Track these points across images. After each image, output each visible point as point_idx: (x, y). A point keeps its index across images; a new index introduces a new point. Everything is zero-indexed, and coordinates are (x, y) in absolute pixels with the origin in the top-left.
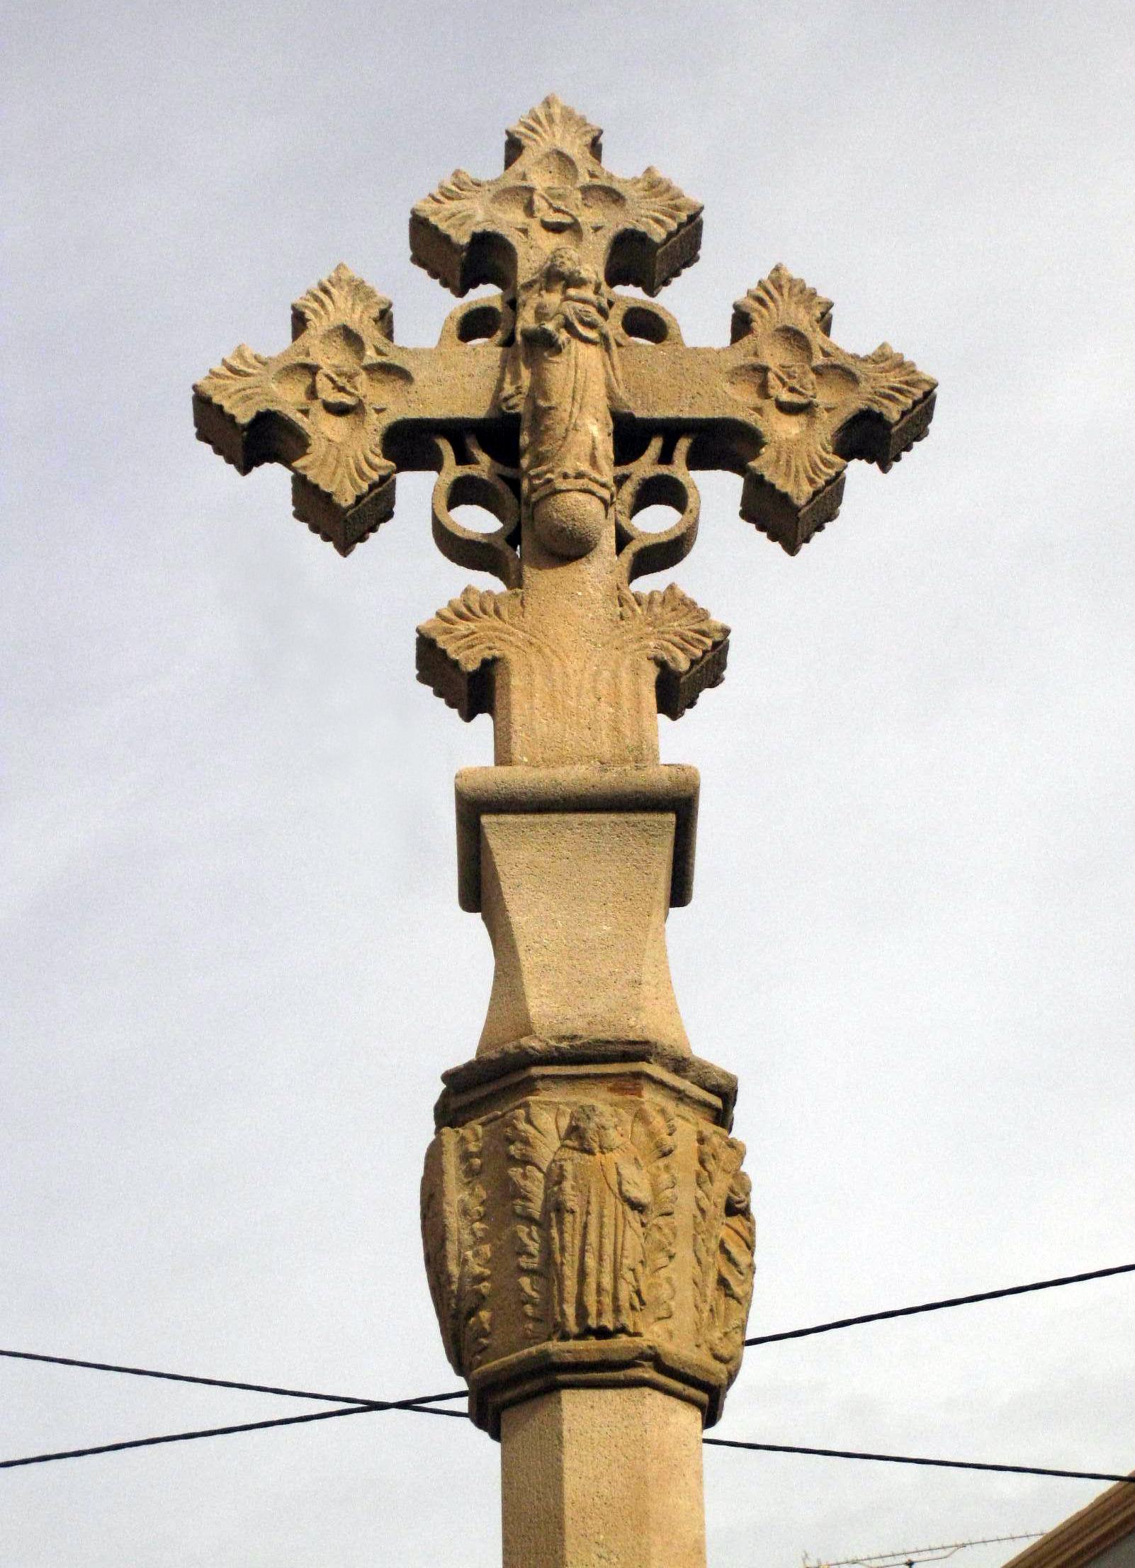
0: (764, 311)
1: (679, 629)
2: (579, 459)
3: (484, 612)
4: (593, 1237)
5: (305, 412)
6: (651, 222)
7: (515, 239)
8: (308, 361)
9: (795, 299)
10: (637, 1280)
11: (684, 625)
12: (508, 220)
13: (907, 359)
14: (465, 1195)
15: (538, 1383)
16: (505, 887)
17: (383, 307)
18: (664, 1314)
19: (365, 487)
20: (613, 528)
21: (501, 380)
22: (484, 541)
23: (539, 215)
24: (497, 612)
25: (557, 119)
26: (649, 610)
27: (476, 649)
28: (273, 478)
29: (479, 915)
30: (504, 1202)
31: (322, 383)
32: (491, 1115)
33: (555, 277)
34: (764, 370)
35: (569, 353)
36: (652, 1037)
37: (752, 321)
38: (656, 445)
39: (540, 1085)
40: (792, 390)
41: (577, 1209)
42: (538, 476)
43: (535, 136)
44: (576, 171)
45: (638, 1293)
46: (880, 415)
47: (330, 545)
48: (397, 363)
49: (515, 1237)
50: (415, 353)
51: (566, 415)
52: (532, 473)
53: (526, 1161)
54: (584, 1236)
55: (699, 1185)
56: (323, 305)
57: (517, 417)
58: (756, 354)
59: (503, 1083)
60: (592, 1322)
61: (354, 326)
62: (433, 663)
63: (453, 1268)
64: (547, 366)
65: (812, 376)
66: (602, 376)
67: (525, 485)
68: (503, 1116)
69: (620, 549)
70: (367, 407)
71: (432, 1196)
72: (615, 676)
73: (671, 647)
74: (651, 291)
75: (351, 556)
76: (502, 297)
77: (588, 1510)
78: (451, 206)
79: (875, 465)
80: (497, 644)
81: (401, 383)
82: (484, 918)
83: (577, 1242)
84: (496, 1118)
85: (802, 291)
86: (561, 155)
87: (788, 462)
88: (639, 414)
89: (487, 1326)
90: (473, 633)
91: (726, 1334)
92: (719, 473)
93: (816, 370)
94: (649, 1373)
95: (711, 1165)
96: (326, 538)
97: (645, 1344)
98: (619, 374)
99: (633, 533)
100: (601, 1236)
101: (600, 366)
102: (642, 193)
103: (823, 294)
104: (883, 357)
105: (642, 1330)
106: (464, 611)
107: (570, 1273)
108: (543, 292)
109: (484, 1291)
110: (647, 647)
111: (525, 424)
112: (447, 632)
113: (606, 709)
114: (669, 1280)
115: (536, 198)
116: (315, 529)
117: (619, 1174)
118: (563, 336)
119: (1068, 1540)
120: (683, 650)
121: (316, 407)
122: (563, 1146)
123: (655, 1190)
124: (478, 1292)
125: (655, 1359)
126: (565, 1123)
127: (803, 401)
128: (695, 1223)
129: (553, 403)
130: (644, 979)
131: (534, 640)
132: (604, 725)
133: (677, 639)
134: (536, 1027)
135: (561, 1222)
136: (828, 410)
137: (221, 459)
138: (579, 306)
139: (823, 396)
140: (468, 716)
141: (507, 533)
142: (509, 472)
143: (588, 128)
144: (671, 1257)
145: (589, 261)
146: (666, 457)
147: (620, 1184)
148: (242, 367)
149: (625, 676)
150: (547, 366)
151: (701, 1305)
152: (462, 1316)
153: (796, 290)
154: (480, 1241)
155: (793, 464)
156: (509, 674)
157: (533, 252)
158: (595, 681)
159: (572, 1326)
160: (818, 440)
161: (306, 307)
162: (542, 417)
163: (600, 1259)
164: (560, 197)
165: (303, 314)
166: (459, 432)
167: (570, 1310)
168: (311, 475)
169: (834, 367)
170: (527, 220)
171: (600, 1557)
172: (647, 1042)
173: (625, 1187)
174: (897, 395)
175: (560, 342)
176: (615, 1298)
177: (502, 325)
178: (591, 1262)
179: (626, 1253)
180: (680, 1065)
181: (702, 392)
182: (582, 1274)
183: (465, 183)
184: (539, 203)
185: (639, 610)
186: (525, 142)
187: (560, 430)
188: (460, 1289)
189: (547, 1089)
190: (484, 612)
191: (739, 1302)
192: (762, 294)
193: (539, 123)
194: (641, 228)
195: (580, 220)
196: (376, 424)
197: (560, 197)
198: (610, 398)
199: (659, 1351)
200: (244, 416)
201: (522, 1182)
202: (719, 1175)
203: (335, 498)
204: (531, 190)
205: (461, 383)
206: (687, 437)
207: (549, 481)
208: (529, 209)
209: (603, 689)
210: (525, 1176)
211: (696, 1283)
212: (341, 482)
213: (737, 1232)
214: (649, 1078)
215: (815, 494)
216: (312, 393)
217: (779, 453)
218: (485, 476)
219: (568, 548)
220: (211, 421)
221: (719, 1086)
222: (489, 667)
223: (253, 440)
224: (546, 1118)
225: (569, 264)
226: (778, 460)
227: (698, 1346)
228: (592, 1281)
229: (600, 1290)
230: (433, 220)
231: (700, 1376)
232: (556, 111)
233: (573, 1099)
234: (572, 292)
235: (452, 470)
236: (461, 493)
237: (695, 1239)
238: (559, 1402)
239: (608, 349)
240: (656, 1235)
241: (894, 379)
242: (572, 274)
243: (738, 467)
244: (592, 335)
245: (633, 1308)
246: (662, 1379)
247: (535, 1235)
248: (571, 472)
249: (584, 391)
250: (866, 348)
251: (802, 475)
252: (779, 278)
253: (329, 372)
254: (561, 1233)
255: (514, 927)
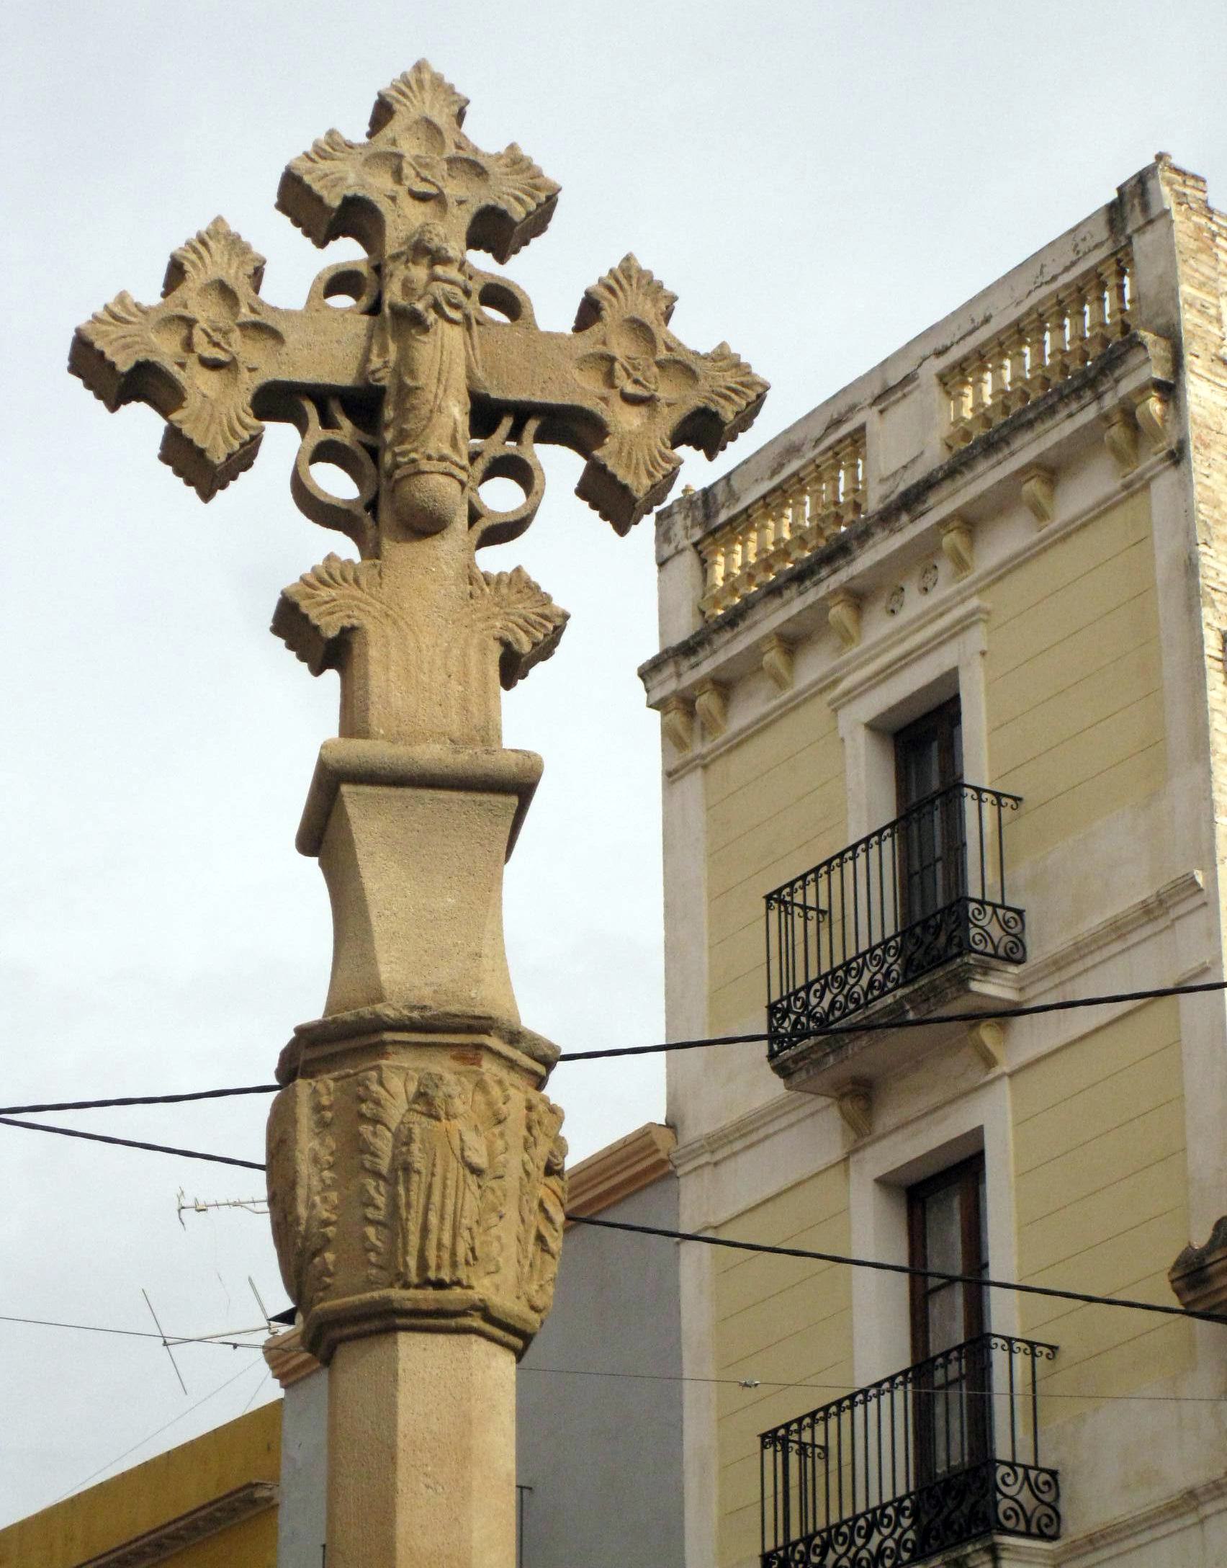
0: (613, 299)
1: (524, 612)
2: (440, 440)
3: (345, 580)
4: (436, 1198)
5: (182, 365)
6: (512, 200)
7: (384, 206)
8: (186, 313)
9: (642, 290)
10: (472, 1238)
11: (527, 608)
12: (377, 186)
13: (743, 360)
14: (315, 1144)
15: (376, 1324)
16: (361, 854)
17: (257, 264)
18: (492, 1269)
19: (236, 445)
20: (466, 507)
21: (368, 351)
22: (344, 507)
23: (407, 183)
24: (356, 581)
25: (427, 84)
26: (497, 590)
27: (335, 616)
28: (142, 422)
29: (315, 860)
30: (353, 1154)
31: (198, 336)
32: (343, 1073)
33: (423, 251)
34: (612, 360)
35: (436, 334)
36: (495, 1013)
37: (601, 309)
38: (507, 424)
39: (390, 1049)
40: (636, 382)
41: (424, 1171)
42: (403, 454)
43: (405, 100)
44: (443, 142)
45: (473, 1250)
46: (716, 415)
47: (192, 490)
48: (270, 323)
49: (363, 1190)
50: (288, 314)
51: (431, 397)
52: (397, 449)
53: (376, 1121)
54: (429, 1196)
55: (526, 1149)
56: (201, 258)
57: (382, 391)
58: (604, 343)
59: (353, 1043)
60: (432, 1275)
61: (230, 282)
62: (291, 622)
63: (302, 1211)
64: (415, 344)
65: (655, 369)
66: (463, 354)
67: (387, 458)
68: (356, 1074)
69: (471, 524)
70: (240, 365)
71: (282, 1142)
72: (464, 655)
73: (516, 629)
74: (501, 258)
75: (116, 413)
76: (368, 262)
77: (418, 1443)
78: (324, 166)
79: (702, 452)
80: (356, 613)
81: (270, 343)
82: (321, 864)
83: (422, 1201)
84: (348, 1076)
85: (650, 282)
86: (429, 123)
87: (629, 453)
88: (495, 395)
89: (331, 1267)
90: (334, 600)
91: (541, 1286)
92: (557, 446)
93: (660, 365)
94: (477, 1322)
95: (536, 1131)
96: (189, 482)
97: (476, 1297)
98: (478, 352)
99: (483, 512)
100: (444, 1196)
101: (462, 347)
102: (505, 170)
103: (669, 287)
104: (723, 357)
105: (474, 1283)
106: (328, 575)
107: (414, 1227)
108: (410, 264)
109: (330, 1235)
110: (493, 627)
111: (391, 397)
112: (311, 597)
113: (456, 688)
114: (499, 1238)
115: (405, 165)
116: (178, 472)
117: (461, 1140)
118: (431, 317)
119: (970, 523)
120: (526, 632)
121: (192, 361)
122: (410, 1110)
123: (491, 1155)
124: (324, 1236)
125: (485, 1311)
126: (413, 1088)
127: (645, 394)
128: (521, 1184)
129: (420, 383)
130: (486, 951)
131: (390, 612)
132: (453, 702)
133: (521, 621)
134: (387, 993)
135: (407, 1182)
136: (669, 405)
137: (90, 393)
138: (448, 287)
139: (665, 390)
140: (317, 670)
141: (366, 500)
142: (367, 439)
143: (456, 98)
144: (501, 1217)
145: (450, 233)
146: (515, 435)
147: (462, 1150)
148: (124, 315)
149: (474, 655)
150: (415, 344)
151: (523, 1261)
152: (308, 1254)
153: (644, 282)
154: (326, 1188)
155: (634, 456)
156: (366, 644)
157: (403, 220)
158: (446, 657)
159: (413, 1278)
160: (658, 433)
161: (185, 258)
162: (407, 395)
163: (442, 1218)
164: (427, 166)
165: (182, 265)
166: (322, 396)
167: (412, 1262)
168: (187, 430)
169: (677, 362)
170: (397, 187)
171: (428, 1487)
172: (490, 1018)
173: (467, 1153)
174: (733, 395)
175: (429, 322)
176: (453, 1254)
177: (368, 290)
178: (433, 1219)
179: (465, 1214)
180: (515, 1037)
181: (553, 377)
182: (425, 1230)
183: (338, 144)
184: (407, 171)
185: (487, 590)
186: (396, 106)
187: (424, 411)
188: (307, 1229)
189: (396, 1053)
190: (345, 580)
191: (553, 1257)
192: (612, 283)
193: (410, 87)
194: (503, 206)
195: (446, 191)
196: (249, 383)
197: (427, 166)
198: (469, 377)
199: (489, 1303)
200: (124, 364)
201: (371, 1139)
202: (541, 1138)
203: (208, 454)
204: (400, 157)
205: (332, 349)
206: (536, 419)
207: (413, 461)
208: (398, 176)
209: (454, 667)
210: (375, 1134)
211: (519, 1241)
212: (214, 438)
213: (554, 1192)
214: (490, 1050)
215: (653, 486)
216: (188, 345)
217: (621, 444)
218: (347, 442)
219: (425, 525)
220: (87, 361)
221: (545, 1056)
222: (347, 635)
223: (115, 375)
224: (397, 1078)
225: (436, 239)
226: (620, 451)
227: (518, 1298)
228: (433, 1238)
229: (440, 1246)
230: (307, 179)
231: (519, 1325)
232: (426, 77)
233: (422, 1065)
234: (439, 270)
235: (318, 433)
236: (324, 453)
237: (520, 1200)
238: (395, 1343)
239: (469, 328)
240: (490, 1196)
241: (730, 380)
242: (438, 250)
243: (584, 451)
244: (456, 315)
245: (467, 1263)
246: (488, 1328)
247: (382, 1189)
248: (434, 455)
249: (446, 367)
250: (705, 346)
251: (642, 467)
252: (629, 269)
253: (205, 326)
254: (408, 1190)
255: (367, 892)
